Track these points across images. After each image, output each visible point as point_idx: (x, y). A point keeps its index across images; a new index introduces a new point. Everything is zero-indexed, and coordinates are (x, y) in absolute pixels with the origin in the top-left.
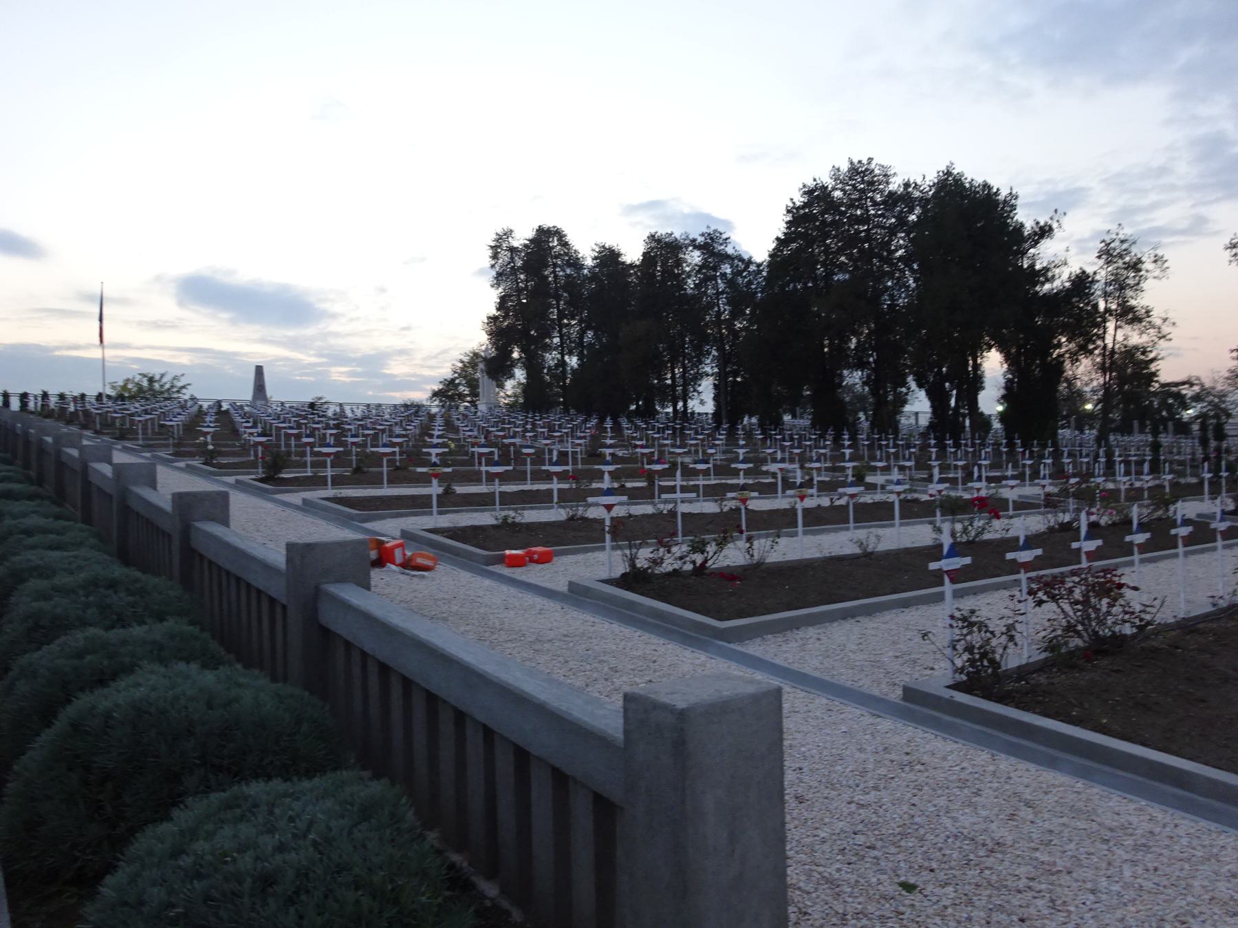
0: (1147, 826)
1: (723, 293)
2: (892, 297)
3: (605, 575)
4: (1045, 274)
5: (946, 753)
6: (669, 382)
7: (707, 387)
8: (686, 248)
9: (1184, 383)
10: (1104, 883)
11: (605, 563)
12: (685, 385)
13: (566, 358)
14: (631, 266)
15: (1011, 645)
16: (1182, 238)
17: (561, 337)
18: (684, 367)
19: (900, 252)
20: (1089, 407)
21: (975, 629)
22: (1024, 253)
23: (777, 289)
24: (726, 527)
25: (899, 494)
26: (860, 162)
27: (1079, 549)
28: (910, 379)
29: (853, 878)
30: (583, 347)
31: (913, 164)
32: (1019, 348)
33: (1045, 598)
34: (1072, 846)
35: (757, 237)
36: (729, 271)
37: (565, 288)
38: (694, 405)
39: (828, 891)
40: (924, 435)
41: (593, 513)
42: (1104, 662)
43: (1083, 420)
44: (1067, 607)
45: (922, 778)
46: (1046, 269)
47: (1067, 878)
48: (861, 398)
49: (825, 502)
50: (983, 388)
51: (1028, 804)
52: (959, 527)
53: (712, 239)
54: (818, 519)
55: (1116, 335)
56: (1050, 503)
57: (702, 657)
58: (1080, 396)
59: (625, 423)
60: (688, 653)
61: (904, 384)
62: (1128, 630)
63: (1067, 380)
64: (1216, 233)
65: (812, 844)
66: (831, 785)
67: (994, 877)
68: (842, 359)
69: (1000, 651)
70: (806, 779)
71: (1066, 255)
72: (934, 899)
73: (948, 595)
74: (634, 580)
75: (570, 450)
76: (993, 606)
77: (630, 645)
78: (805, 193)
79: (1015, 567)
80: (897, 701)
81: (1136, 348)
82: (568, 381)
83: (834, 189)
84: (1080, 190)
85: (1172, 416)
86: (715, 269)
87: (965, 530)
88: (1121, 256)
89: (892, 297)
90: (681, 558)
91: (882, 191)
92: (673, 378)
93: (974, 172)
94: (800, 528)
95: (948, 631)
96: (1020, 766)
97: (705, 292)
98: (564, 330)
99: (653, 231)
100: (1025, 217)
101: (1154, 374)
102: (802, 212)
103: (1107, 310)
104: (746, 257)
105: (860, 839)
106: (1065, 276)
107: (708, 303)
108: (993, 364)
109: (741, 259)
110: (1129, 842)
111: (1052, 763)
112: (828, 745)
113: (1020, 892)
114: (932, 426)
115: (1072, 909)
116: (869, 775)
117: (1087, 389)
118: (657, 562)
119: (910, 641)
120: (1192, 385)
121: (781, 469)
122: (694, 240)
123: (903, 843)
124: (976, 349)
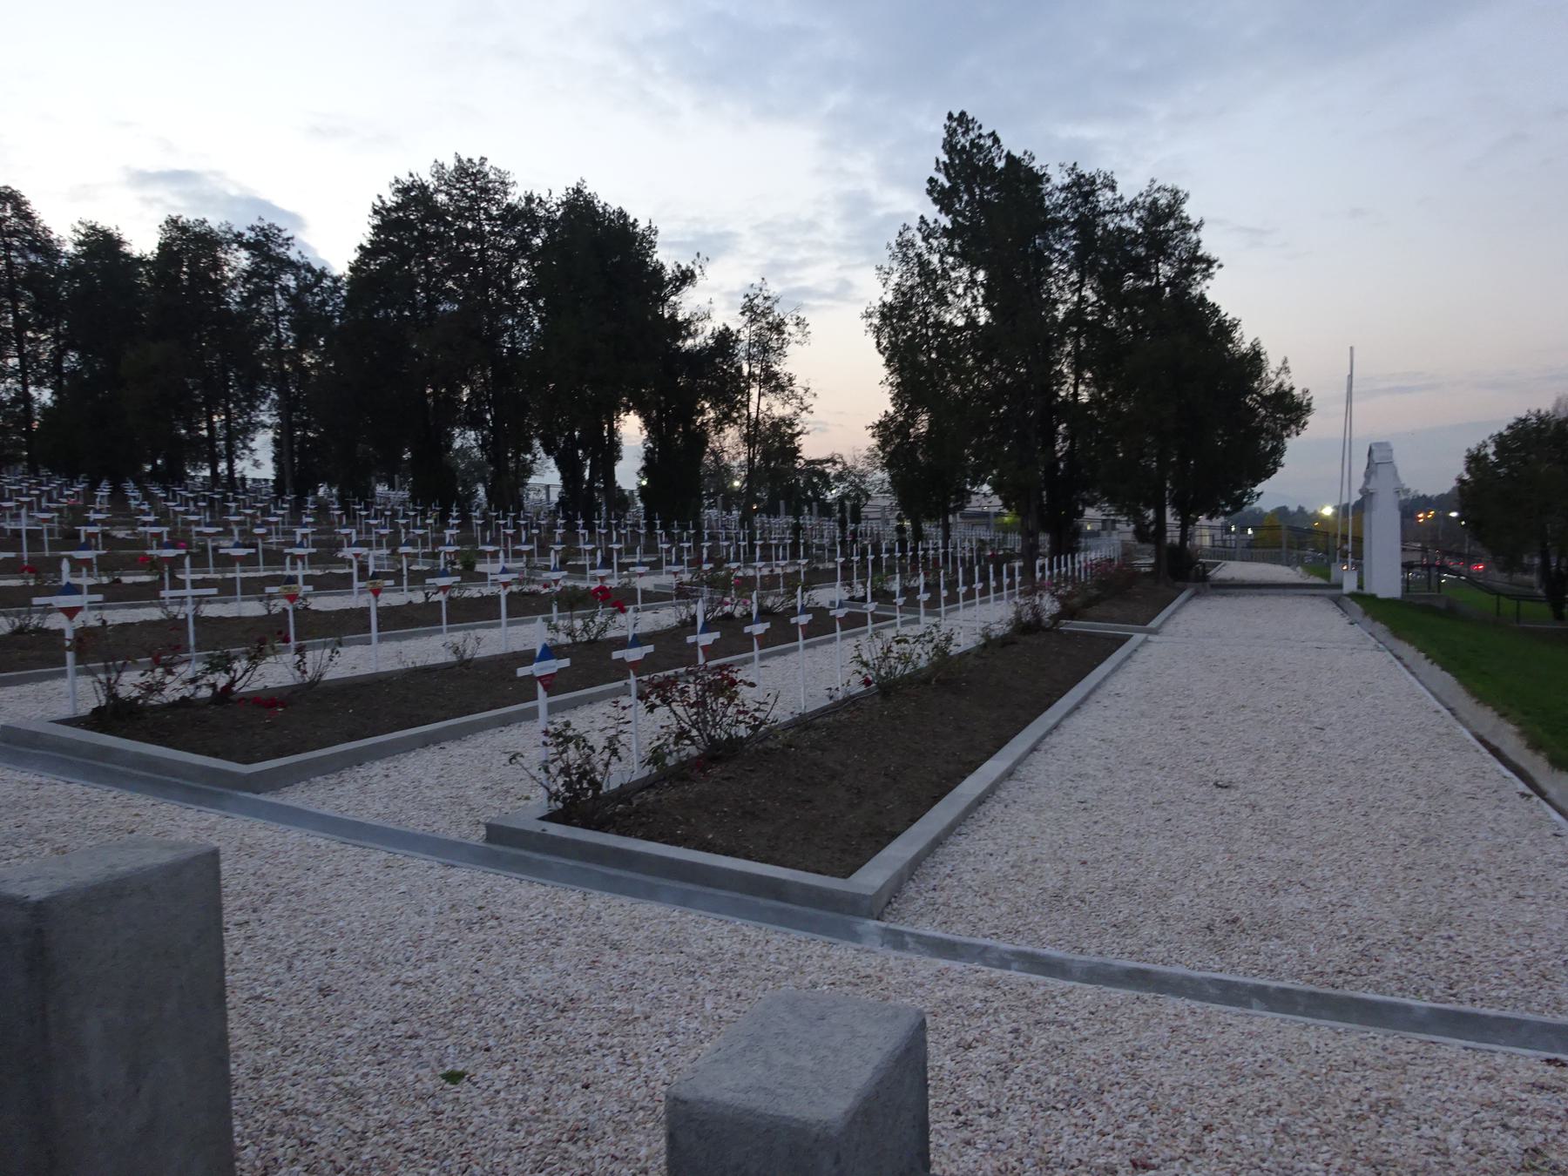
0: (737, 948)
1: (283, 313)
2: (512, 337)
3: (66, 711)
4: (680, 328)
5: (525, 898)
6: (205, 433)
7: (263, 443)
8: (229, 244)
9: (827, 461)
10: (683, 1021)
11: (76, 691)
12: (230, 439)
13: (32, 390)
14: (140, 261)
15: (614, 759)
16: (829, 302)
17: (22, 357)
18: (228, 412)
19: (523, 283)
20: (737, 484)
21: (572, 746)
22: (665, 300)
23: (361, 315)
24: (262, 637)
25: (506, 585)
26: (470, 160)
27: (695, 644)
28: (537, 443)
29: (381, 1081)
30: (62, 375)
31: (537, 174)
32: (660, 412)
33: (658, 702)
34: (655, 986)
35: (334, 241)
36: (292, 284)
37: (28, 283)
38: (243, 467)
39: (346, 1107)
40: (554, 514)
41: (56, 622)
42: (716, 771)
43: (729, 499)
44: (680, 710)
45: (493, 936)
46: (688, 322)
47: (645, 1024)
48: (478, 466)
49: (418, 598)
50: (620, 458)
51: (614, 946)
52: (578, 624)
53: (266, 236)
54: (399, 621)
55: (763, 404)
56: (683, 593)
57: (213, 816)
58: (724, 472)
59: (131, 489)
60: (191, 814)
61: (529, 449)
62: (743, 731)
63: (713, 452)
64: (861, 301)
65: (333, 1049)
66: (373, 965)
67: (562, 1042)
68: (450, 414)
69: (600, 768)
70: (338, 962)
71: (709, 306)
72: (484, 1085)
73: (543, 711)
74: (115, 716)
75: (24, 527)
76: (592, 720)
77: (94, 811)
78: (398, 190)
79: (622, 669)
80: (481, 843)
81: (782, 419)
82: (36, 425)
83: (437, 191)
84: (729, 234)
85: (817, 495)
86: (272, 278)
87: (586, 628)
88: (764, 314)
89: (512, 337)
90: (193, 681)
91: (498, 203)
92: (211, 427)
93: (609, 195)
94: (374, 633)
95: (542, 750)
96: (615, 902)
97: (258, 311)
98: (28, 348)
99: (174, 215)
100: (666, 257)
101: (797, 450)
102: (394, 215)
103: (751, 374)
104: (317, 267)
105: (402, 1028)
106: (708, 332)
107: (262, 325)
108: (631, 429)
109: (309, 269)
110: (716, 969)
111: (651, 894)
112: (377, 913)
113: (588, 1053)
114: (562, 502)
115: (643, 1060)
116: (426, 943)
117: (735, 464)
118: (151, 689)
119: (495, 770)
120: (835, 463)
121: (357, 555)
122: (240, 235)
123: (455, 1023)
124: (610, 411)
